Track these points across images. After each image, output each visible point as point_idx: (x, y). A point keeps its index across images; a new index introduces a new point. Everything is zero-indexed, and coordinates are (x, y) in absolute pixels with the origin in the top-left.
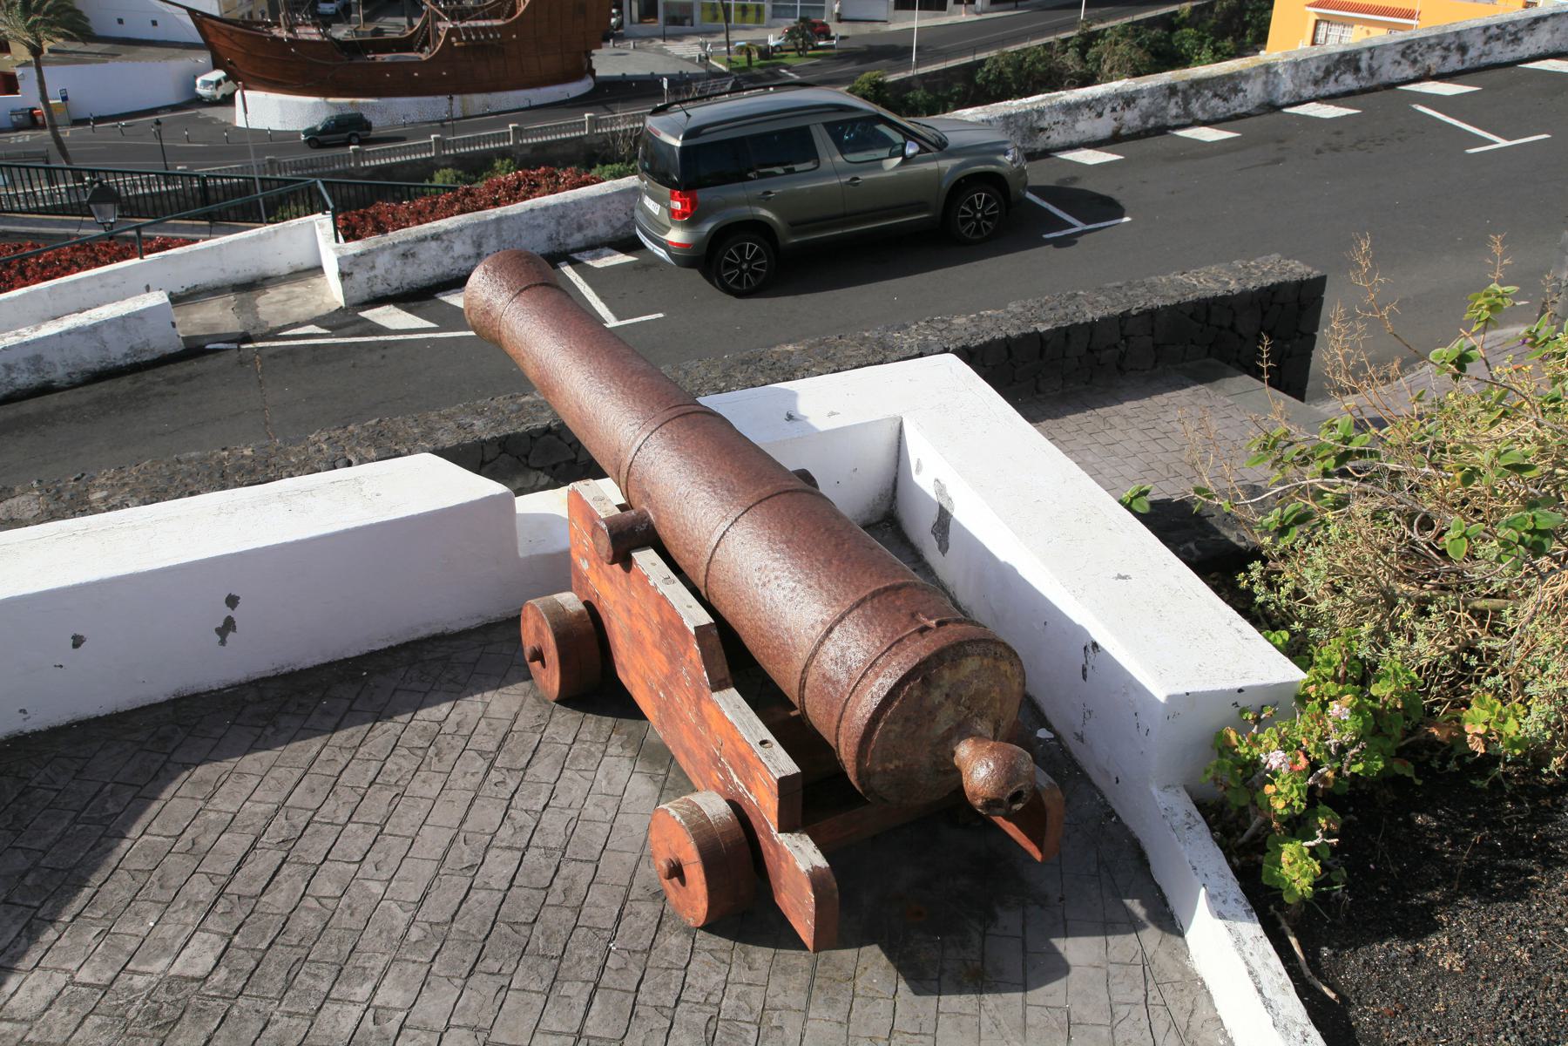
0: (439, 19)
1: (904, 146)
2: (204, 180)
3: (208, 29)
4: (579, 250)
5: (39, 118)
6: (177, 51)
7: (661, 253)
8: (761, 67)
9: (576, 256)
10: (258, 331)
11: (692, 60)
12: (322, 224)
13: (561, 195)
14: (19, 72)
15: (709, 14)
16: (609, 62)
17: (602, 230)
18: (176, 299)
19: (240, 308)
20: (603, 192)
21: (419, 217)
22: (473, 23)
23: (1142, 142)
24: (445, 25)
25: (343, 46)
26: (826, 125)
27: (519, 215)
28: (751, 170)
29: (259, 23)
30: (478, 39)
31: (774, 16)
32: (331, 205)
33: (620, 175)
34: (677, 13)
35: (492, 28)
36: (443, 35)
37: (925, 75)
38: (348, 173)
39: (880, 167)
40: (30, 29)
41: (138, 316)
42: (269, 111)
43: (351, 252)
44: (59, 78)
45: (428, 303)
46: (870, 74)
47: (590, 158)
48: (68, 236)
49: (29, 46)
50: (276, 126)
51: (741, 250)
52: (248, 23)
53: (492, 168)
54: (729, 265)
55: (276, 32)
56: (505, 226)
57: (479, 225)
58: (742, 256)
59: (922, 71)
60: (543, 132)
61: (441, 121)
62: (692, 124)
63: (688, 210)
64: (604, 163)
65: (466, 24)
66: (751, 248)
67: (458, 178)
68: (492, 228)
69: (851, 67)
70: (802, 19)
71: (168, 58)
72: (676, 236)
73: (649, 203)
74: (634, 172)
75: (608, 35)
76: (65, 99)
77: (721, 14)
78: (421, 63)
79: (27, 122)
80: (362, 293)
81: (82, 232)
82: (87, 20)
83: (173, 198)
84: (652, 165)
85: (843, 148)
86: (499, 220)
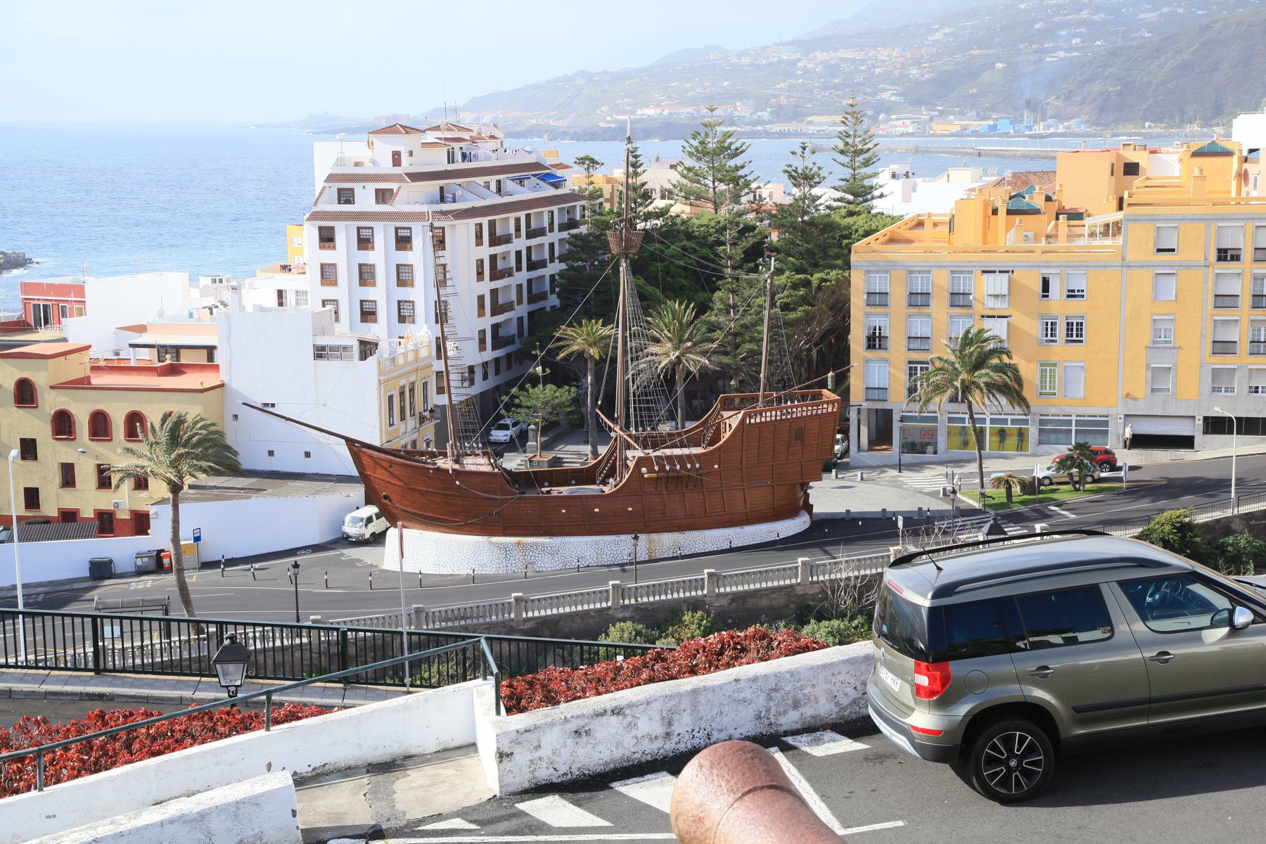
0: (629, 447)
1: (1231, 612)
2: (344, 634)
3: (366, 460)
4: (794, 733)
5: (166, 561)
6: (327, 485)
7: (902, 741)
8: (1023, 503)
9: (789, 740)
10: (393, 824)
11: (934, 494)
12: (480, 692)
13: (773, 662)
14: (152, 510)
15: (958, 440)
16: (829, 496)
17: (824, 708)
18: (301, 781)
19: (373, 794)
20: (827, 660)
21: (599, 686)
22: (668, 452)
24: (635, 454)
25: (516, 478)
26: (1123, 584)
27: (721, 687)
28: (1023, 638)
29: (422, 454)
31: (1040, 443)
32: (495, 670)
33: (843, 639)
34: (917, 439)
35: (689, 457)
36: (631, 464)
37: (1248, 517)
39: (1199, 640)
40: (174, 464)
41: (254, 802)
42: (430, 554)
43: (514, 727)
44: (194, 515)
45: (601, 794)
46: (1171, 512)
47: (802, 613)
48: (181, 701)
49: (169, 482)
50: (428, 569)
51: (1008, 741)
52: (410, 454)
53: (681, 622)
54: (991, 761)
55: (442, 463)
56: (702, 699)
57: (670, 697)
58: (1010, 749)
59: (1244, 509)
60: (745, 578)
61: (622, 565)
62: (944, 579)
63: (937, 686)
64: (819, 620)
65: (658, 453)
66: (1022, 740)
67: (638, 633)
68: (686, 703)
69: (1144, 504)
70: (1079, 446)
71: (317, 492)
72: (924, 718)
73: (887, 677)
74: (865, 636)
75: (830, 465)
76: (197, 539)
77: (973, 439)
78: (602, 497)
79: (152, 564)
80: (522, 779)
81: (199, 695)
82: (236, 454)
83: (297, 654)
84: (891, 629)
85: (1145, 612)
86: (695, 692)
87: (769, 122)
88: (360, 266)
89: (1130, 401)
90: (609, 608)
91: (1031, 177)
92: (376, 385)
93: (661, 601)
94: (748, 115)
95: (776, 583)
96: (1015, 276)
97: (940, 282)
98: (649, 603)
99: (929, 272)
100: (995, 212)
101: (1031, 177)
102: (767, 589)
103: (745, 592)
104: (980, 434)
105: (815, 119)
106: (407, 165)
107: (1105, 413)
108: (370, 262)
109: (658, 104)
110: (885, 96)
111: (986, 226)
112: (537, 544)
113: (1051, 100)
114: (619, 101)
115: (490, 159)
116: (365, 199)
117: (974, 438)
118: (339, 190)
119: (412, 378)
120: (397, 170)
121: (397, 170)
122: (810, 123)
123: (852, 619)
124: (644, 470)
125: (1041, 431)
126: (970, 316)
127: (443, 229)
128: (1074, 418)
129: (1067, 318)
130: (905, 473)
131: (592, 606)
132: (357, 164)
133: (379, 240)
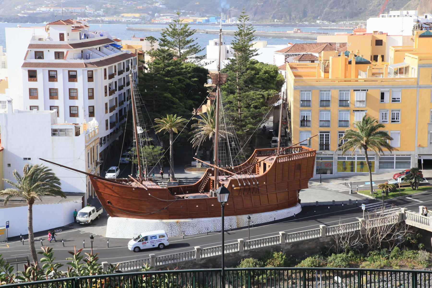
16: (309, 195)
23: (377, 175)
30: (247, 185)
31: (380, 167)
34: (323, 167)
38: (194, 264)
53: (272, 257)
76: (8, 226)
77: (349, 167)
87: (104, 16)
88: (50, 89)
89: (421, 148)
90: (238, 252)
91: (305, 45)
92: (84, 147)
93: (261, 248)
94: (92, 12)
95: (311, 237)
96: (369, 92)
97: (334, 95)
98: (256, 249)
99: (330, 91)
100: (350, 63)
101: (305, 45)
102: (307, 240)
103: (297, 242)
104: (352, 164)
105: (125, 15)
106: (66, 41)
107: (409, 154)
108: (56, 87)
109: (47, 6)
110: (157, 5)
111: (346, 69)
112: (186, 222)
113: (232, 8)
114: (26, 4)
115: (94, 37)
116: (49, 57)
117: (367, 166)
118: (36, 52)
119: (94, 144)
120: (62, 43)
121: (62, 43)
122: (123, 17)
123: (348, 253)
124: (233, 186)
125: (380, 162)
126: (348, 111)
127: (92, 71)
128: (395, 156)
129: (392, 111)
130: (323, 183)
131: (231, 251)
132: (40, 39)
133: (60, 77)
